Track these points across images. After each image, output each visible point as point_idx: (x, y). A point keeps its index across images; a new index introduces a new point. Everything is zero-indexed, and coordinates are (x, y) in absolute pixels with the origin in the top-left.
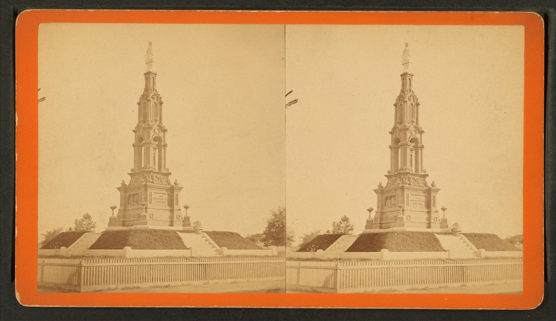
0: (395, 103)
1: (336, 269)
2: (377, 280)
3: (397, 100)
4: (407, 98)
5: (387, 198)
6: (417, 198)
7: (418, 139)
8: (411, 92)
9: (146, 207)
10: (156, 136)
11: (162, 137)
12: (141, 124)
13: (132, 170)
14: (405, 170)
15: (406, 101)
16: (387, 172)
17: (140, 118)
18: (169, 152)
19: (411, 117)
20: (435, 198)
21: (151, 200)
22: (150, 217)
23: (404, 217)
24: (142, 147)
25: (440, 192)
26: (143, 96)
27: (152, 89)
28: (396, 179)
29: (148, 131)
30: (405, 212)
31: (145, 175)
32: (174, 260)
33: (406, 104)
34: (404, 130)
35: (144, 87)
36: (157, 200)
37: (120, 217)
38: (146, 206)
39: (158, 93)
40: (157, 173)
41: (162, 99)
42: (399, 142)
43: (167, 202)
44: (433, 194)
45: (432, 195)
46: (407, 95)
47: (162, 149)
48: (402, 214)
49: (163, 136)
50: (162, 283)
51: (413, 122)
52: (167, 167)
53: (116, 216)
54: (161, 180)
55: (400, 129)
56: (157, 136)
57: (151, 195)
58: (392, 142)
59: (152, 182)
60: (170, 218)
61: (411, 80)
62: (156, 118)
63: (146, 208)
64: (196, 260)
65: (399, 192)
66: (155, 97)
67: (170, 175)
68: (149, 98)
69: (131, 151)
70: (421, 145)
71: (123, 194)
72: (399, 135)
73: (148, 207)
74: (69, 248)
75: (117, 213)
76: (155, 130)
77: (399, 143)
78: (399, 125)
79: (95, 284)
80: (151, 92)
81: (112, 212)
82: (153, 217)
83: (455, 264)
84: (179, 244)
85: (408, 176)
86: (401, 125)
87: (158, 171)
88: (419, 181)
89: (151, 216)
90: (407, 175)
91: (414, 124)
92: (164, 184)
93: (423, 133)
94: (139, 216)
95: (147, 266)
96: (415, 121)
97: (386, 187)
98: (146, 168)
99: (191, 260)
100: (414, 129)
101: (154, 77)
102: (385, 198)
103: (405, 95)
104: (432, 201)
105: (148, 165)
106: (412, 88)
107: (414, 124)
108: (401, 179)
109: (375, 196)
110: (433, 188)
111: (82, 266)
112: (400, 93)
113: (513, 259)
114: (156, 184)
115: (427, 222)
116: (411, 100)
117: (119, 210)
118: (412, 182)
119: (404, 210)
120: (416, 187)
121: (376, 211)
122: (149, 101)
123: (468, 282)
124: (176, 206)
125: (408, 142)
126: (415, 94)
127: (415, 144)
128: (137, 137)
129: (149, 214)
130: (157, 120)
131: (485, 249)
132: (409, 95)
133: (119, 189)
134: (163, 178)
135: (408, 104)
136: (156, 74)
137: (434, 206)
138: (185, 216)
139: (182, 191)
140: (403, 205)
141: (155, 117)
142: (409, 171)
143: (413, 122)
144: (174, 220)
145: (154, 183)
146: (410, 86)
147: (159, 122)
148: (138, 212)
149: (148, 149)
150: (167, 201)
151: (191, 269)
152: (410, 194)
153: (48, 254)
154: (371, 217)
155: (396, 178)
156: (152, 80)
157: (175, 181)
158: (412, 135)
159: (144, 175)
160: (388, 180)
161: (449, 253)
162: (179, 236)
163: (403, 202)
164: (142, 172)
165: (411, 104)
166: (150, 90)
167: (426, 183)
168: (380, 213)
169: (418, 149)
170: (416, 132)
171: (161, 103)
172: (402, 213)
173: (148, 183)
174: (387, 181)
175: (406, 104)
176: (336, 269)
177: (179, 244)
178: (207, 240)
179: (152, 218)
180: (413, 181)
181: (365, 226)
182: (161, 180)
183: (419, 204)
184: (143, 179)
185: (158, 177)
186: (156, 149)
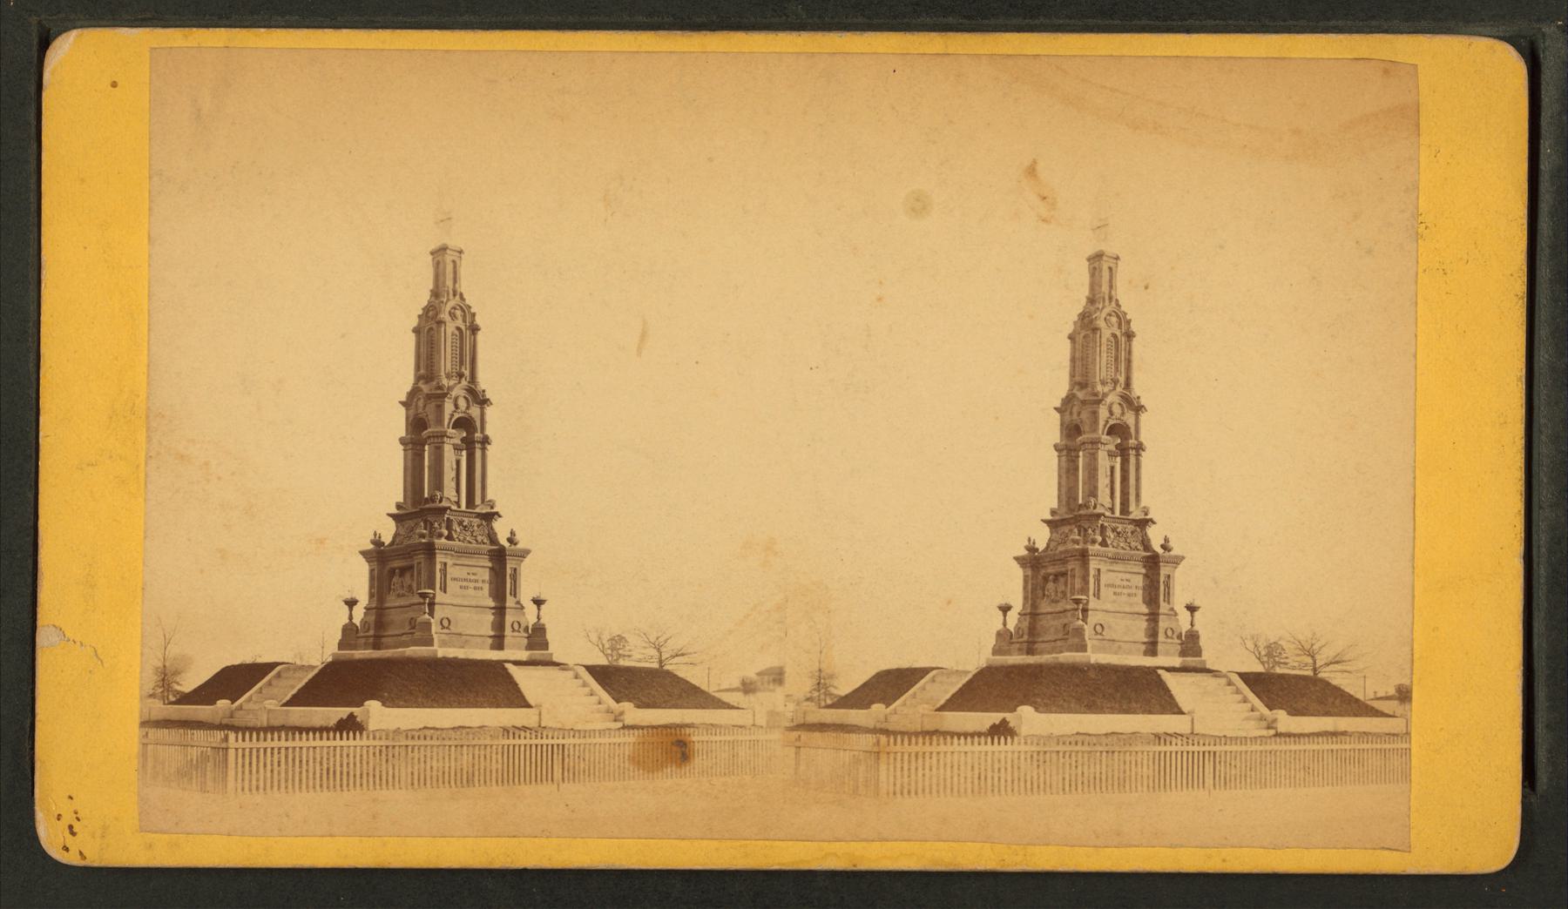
1: (878, 753)
4: (447, 313)
5: (1046, 579)
6: (1122, 580)
7: (475, 422)
11: (476, 419)
20: (1171, 580)
21: (1099, 590)
22: (513, 628)
23: (432, 620)
24: (1079, 451)
25: (529, 557)
26: (426, 310)
29: (439, 403)
30: (437, 607)
32: (720, 733)
33: (1098, 336)
34: (435, 398)
35: (431, 287)
37: (1023, 631)
41: (476, 318)
42: (426, 429)
43: (486, 587)
45: (1164, 571)
46: (446, 304)
47: (477, 450)
48: (1083, 620)
50: (456, 790)
51: (461, 376)
52: (490, 496)
54: (472, 532)
55: (427, 394)
56: (1118, 422)
57: (444, 571)
58: (1062, 432)
59: (449, 538)
61: (1114, 272)
62: (460, 368)
63: (1085, 611)
64: (528, 735)
65: (420, 558)
66: (458, 313)
67: (496, 516)
68: (442, 316)
69: (1052, 459)
70: (1136, 442)
71: (1029, 573)
72: (424, 409)
73: (437, 601)
76: (456, 399)
77: (1080, 438)
78: (1078, 390)
79: (909, 792)
81: (1002, 618)
85: (1100, 522)
87: (467, 507)
88: (476, 528)
89: (445, 623)
90: (1098, 520)
91: (464, 383)
92: (480, 541)
93: (1143, 412)
94: (412, 623)
96: (467, 373)
97: (1043, 551)
98: (1088, 508)
99: (514, 734)
100: (1118, 401)
101: (1113, 266)
102: (389, 571)
104: (1162, 588)
106: (460, 287)
107: (464, 383)
109: (1018, 573)
110: (1167, 554)
116: (457, 318)
117: (365, 608)
119: (434, 604)
121: (1018, 611)
122: (440, 323)
123: (1217, 790)
124: (442, 593)
125: (1103, 434)
126: (467, 302)
127: (467, 435)
130: (1118, 381)
132: (452, 303)
133: (364, 553)
134: (1132, 533)
135: (447, 328)
136: (1117, 258)
139: (1180, 566)
143: (461, 376)
146: (455, 281)
148: (411, 614)
149: (1093, 457)
150: (488, 585)
152: (450, 562)
153: (970, 728)
154: (1008, 627)
155: (415, 521)
156: (1106, 274)
158: (1114, 417)
160: (397, 527)
161: (1193, 719)
163: (1085, 590)
164: (422, 510)
165: (1114, 336)
167: (1149, 540)
168: (374, 611)
170: (1123, 410)
171: (1130, 336)
172: (1081, 617)
173: (436, 541)
174: (395, 529)
175: (443, 329)
176: (878, 753)
177: (514, 697)
178: (585, 685)
179: (448, 628)
180: (458, 530)
182: (472, 532)
183: (1129, 595)
184: (425, 529)
185: (465, 524)
186: (462, 450)
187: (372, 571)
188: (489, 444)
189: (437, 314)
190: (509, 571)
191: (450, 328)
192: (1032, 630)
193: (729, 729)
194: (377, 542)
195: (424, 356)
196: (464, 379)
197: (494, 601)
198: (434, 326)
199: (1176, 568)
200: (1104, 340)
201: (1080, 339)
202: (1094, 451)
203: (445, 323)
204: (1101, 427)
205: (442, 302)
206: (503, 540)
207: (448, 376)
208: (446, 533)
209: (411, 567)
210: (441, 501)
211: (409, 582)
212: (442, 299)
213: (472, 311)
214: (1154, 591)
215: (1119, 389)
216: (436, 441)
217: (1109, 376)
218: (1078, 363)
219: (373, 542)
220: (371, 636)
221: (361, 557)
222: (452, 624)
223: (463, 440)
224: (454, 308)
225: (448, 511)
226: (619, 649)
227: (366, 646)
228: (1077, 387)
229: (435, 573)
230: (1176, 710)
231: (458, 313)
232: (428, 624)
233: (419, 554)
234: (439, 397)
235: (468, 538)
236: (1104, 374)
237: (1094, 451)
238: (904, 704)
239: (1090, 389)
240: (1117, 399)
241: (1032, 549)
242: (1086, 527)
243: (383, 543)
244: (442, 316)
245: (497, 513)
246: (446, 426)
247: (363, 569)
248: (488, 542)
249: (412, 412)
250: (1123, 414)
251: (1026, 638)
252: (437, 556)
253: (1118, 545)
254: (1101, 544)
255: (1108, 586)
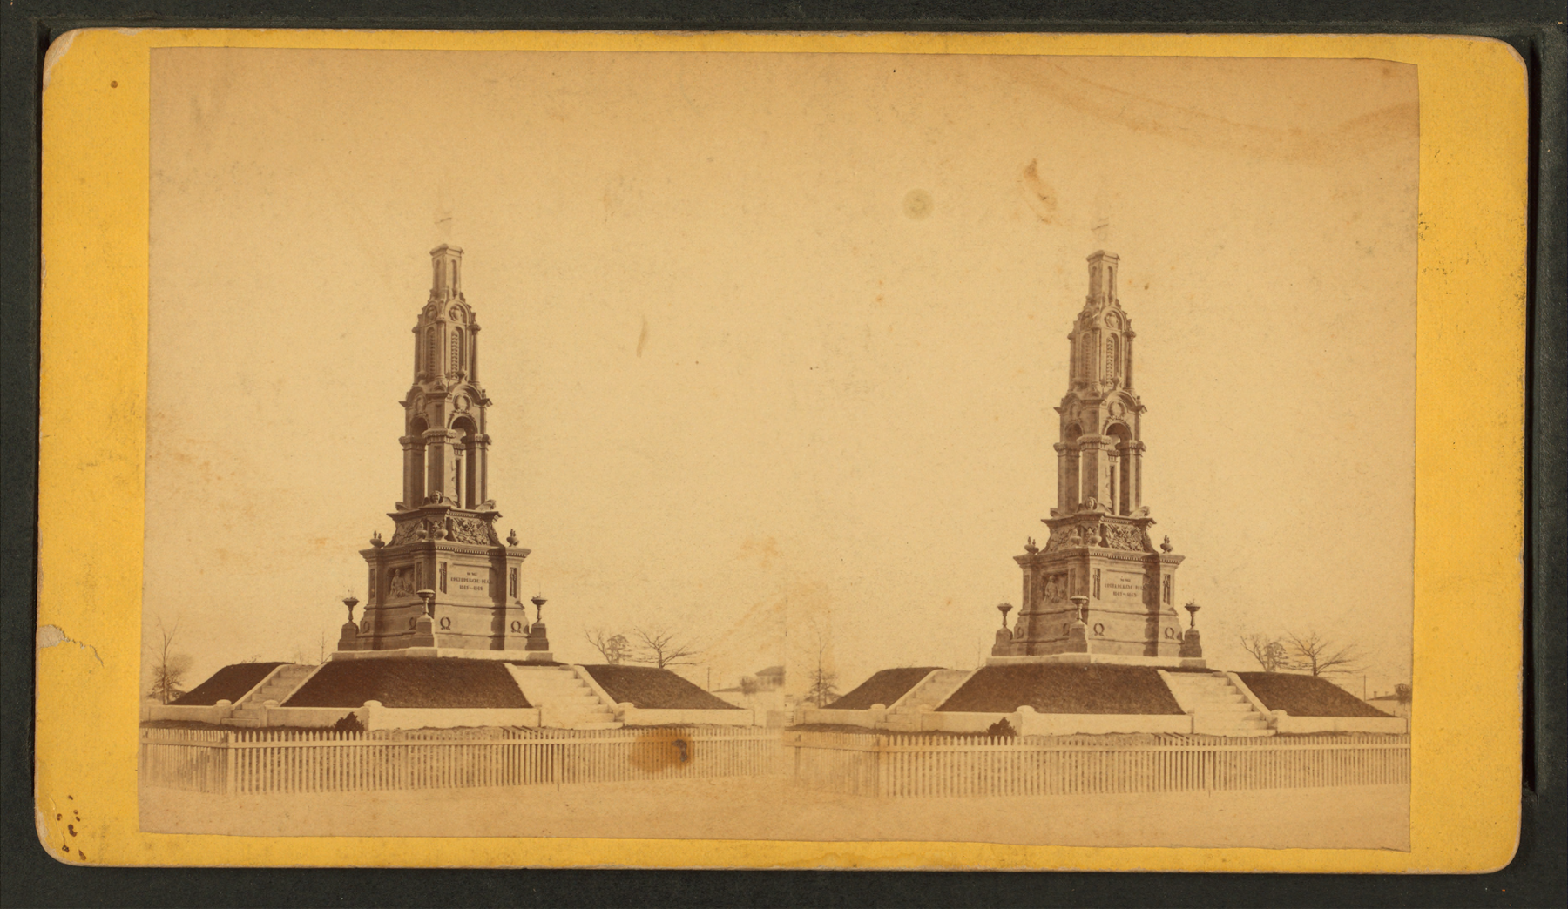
0: (1071, 331)
2: (279, 781)
3: (419, 316)
4: (447, 313)
5: (392, 572)
6: (1122, 580)
7: (475, 421)
8: (458, 297)
9: (1085, 607)
10: (461, 415)
11: (476, 419)
12: (421, 384)
13: (399, 506)
14: (438, 501)
15: (1098, 326)
16: (1048, 512)
17: (1074, 377)
18: (1151, 466)
19: (458, 364)
21: (1099, 590)
23: (432, 620)
25: (529, 557)
26: (426, 310)
27: (1107, 297)
28: (417, 524)
29: (438, 403)
30: (437, 607)
31: (430, 518)
33: (1098, 336)
34: (434, 398)
36: (461, 583)
38: (430, 598)
39: (467, 302)
40: (1118, 518)
41: (1132, 324)
42: (426, 429)
43: (486, 587)
44: (1164, 571)
47: (1131, 456)
48: (1082, 620)
49: (1134, 422)
51: (461, 376)
52: (489, 496)
53: (1012, 630)
55: (427, 395)
56: (1118, 422)
57: (444, 571)
59: (449, 538)
60: (1146, 636)
61: (1114, 271)
62: (460, 368)
63: (1085, 611)
64: (528, 735)
66: (458, 313)
68: (442, 316)
69: (1052, 460)
70: (1136, 442)
71: (1029, 572)
74: (892, 707)
75: (362, 616)
76: (456, 399)
77: (425, 432)
80: (448, 300)
81: (1002, 618)
82: (1104, 633)
83: (1193, 745)
84: (514, 697)
86: (431, 383)
87: (467, 508)
88: (476, 528)
89: (445, 623)
91: (464, 383)
95: (441, 748)
96: (467, 373)
97: (1043, 551)
100: (463, 395)
103: (441, 305)
105: (438, 494)
106: (460, 287)
107: (464, 383)
108: (428, 523)
109: (1018, 573)
110: (1167, 554)
111: (231, 746)
112: (428, 298)
113: (638, 729)
114: (459, 541)
115: (492, 633)
118: (456, 531)
120: (466, 544)
122: (440, 323)
123: (1217, 790)
128: (411, 419)
129: (1093, 626)
131: (635, 704)
132: (451, 304)
133: (364, 553)
134: (1132, 533)
136: (1117, 258)
137: (1168, 600)
138: (1189, 630)
140: (432, 591)
141: (458, 368)
142: (448, 505)
143: (461, 376)
144: (506, 633)
145: (1107, 546)
146: (455, 281)
147: (468, 379)
149: (1093, 459)
150: (1141, 592)
151: (1198, 761)
152: (450, 562)
154: (1008, 627)
157: (509, 536)
158: (459, 410)
159: (1083, 525)
160: (397, 527)
161: (1193, 719)
162: (508, 674)
163: (1084, 590)
165: (1114, 336)
166: (1099, 303)
167: (1149, 540)
168: (374, 611)
169: (475, 448)
170: (1123, 410)
174: (395, 529)
177: (514, 697)
179: (447, 628)
180: (458, 530)
181: (339, 644)
183: (1129, 595)
184: (425, 529)
185: (464, 524)
187: (372, 571)
188: (489, 444)
189: (437, 314)
190: (509, 571)
191: (450, 327)
192: (1032, 630)
193: (729, 729)
194: (377, 543)
195: (423, 357)
196: (463, 379)
197: (493, 601)
198: (434, 326)
199: (522, 561)
200: (1104, 340)
201: (1079, 339)
202: (1094, 451)
203: (445, 323)
204: (1101, 427)
205: (443, 302)
206: (503, 540)
207: (448, 376)
208: (446, 532)
209: (411, 567)
210: (441, 501)
211: (1063, 588)
212: (442, 299)
213: (472, 311)
214: (1154, 591)
215: (1119, 389)
216: (436, 441)
217: (454, 370)
218: (1078, 363)
219: (373, 542)
220: (371, 636)
221: (361, 557)
222: (452, 623)
223: (463, 440)
224: (455, 308)
225: (448, 511)
226: (619, 649)
227: (366, 646)
228: (1077, 387)
229: (435, 573)
230: (1176, 710)
231: (458, 313)
232: (428, 624)
233: (420, 554)
234: (438, 397)
235: (468, 538)
236: (1104, 374)
237: (1094, 451)
238: (904, 704)
239: (1089, 389)
240: (1117, 400)
241: (1032, 549)
242: (1086, 527)
243: (383, 543)
244: (442, 316)
245: (497, 513)
246: (446, 426)
247: (362, 569)
248: (488, 542)
249: (412, 412)
250: (1123, 414)
251: (1026, 638)
252: (437, 556)
253: (465, 539)
254: (1101, 544)
255: (1108, 586)
